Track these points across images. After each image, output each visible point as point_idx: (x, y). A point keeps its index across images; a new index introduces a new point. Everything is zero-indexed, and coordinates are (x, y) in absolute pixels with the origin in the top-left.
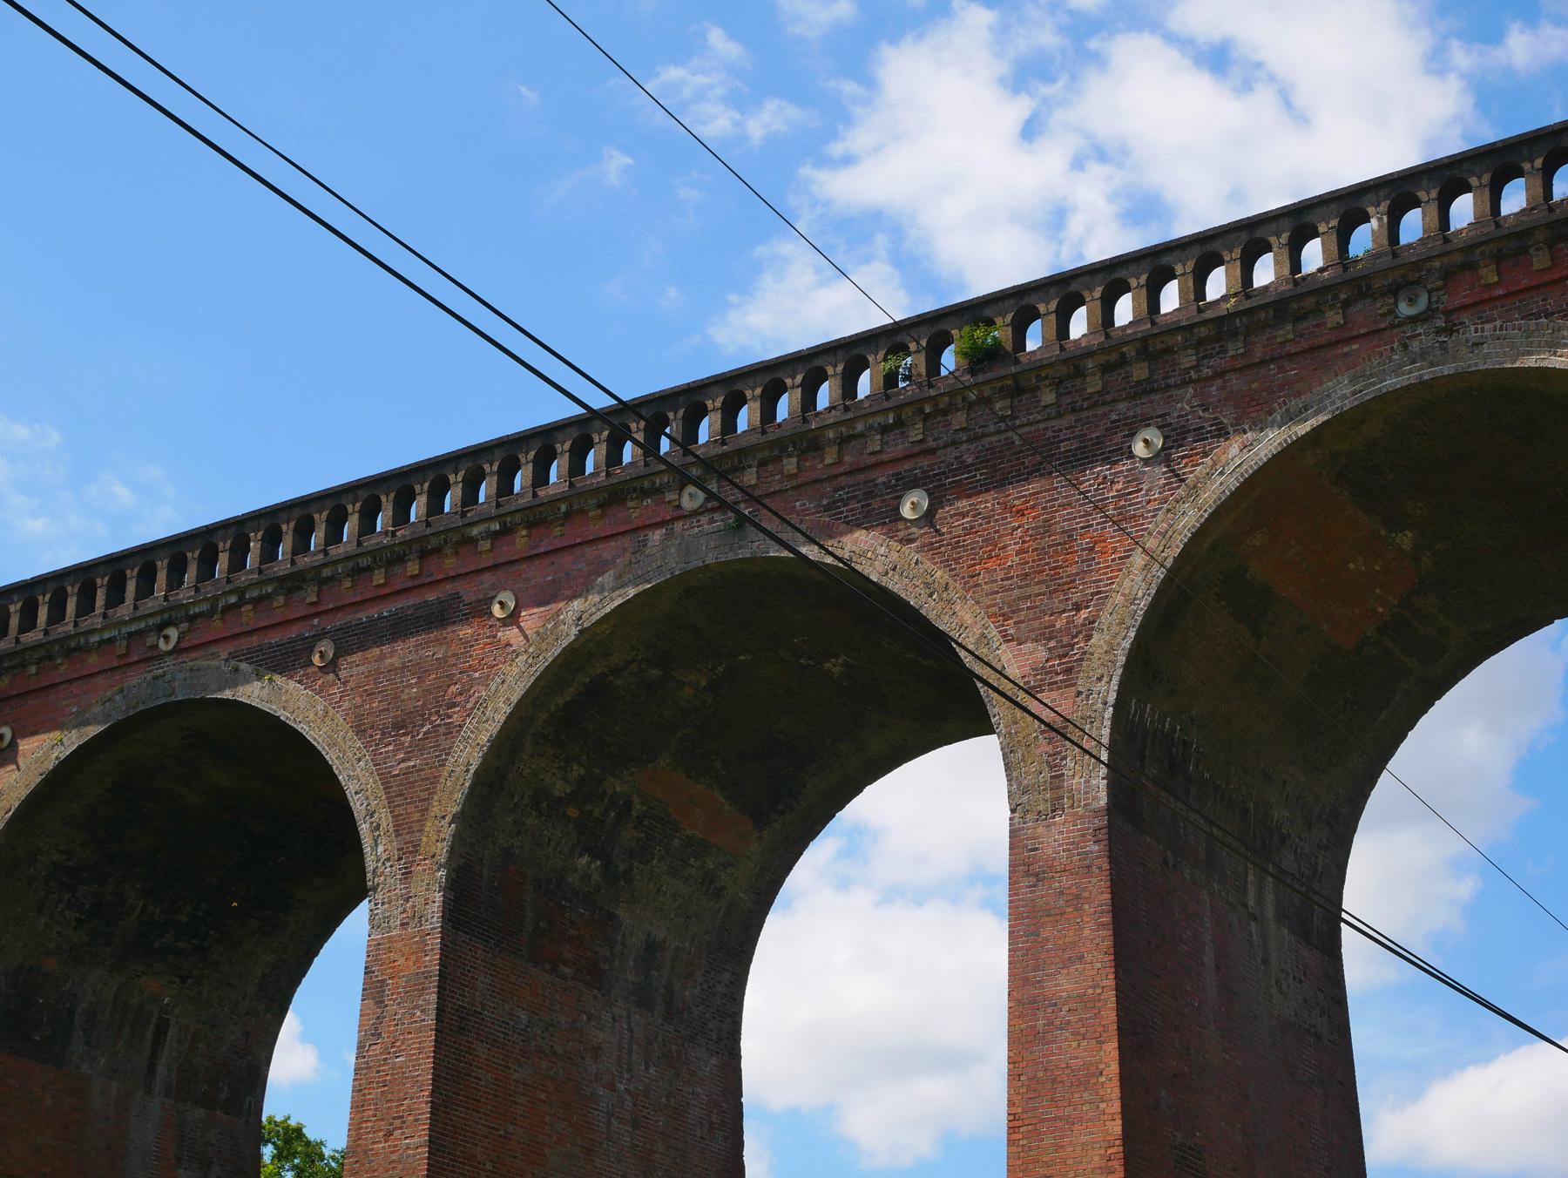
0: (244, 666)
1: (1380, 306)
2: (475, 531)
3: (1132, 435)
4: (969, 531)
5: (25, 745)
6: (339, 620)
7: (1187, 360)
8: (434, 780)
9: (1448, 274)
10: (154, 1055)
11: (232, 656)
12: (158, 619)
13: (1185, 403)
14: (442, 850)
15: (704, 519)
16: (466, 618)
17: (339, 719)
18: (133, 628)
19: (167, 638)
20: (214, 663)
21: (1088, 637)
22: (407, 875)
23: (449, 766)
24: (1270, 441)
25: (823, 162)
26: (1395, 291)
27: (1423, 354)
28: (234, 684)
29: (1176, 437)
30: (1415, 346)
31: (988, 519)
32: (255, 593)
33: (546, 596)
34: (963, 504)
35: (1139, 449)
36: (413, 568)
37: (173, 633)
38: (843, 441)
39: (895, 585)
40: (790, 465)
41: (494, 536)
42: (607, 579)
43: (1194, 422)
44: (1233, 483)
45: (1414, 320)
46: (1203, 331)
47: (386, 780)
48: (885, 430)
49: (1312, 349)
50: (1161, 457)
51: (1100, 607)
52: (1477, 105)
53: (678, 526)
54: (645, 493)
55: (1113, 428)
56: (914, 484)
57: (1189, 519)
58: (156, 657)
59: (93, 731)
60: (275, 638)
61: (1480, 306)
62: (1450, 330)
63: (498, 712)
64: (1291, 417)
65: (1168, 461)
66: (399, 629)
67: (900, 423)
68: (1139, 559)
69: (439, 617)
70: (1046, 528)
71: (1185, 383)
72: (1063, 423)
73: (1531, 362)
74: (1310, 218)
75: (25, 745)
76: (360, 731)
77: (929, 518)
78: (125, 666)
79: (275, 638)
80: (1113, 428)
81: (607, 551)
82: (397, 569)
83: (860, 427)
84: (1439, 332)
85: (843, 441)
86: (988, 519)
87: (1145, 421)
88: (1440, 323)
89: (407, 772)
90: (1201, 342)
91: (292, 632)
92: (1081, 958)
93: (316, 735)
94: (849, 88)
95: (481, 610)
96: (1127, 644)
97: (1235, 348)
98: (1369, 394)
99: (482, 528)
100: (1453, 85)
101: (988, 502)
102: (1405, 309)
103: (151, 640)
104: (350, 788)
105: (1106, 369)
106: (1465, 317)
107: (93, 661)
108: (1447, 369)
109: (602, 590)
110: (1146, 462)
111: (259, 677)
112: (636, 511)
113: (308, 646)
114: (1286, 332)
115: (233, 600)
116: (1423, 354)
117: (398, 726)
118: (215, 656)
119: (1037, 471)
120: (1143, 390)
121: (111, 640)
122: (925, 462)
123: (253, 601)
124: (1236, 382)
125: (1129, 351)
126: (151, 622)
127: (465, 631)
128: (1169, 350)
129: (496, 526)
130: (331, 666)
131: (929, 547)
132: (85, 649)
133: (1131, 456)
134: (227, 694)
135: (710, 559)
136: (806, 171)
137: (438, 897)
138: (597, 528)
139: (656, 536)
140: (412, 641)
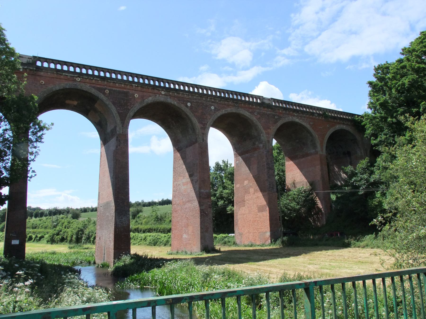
6: (111, 88)
15: (164, 96)
19: (78, 79)
37: (79, 79)
53: (160, 95)
79: (98, 86)
81: (151, 94)
87: (213, 105)
120: (213, 102)
139: (158, 95)
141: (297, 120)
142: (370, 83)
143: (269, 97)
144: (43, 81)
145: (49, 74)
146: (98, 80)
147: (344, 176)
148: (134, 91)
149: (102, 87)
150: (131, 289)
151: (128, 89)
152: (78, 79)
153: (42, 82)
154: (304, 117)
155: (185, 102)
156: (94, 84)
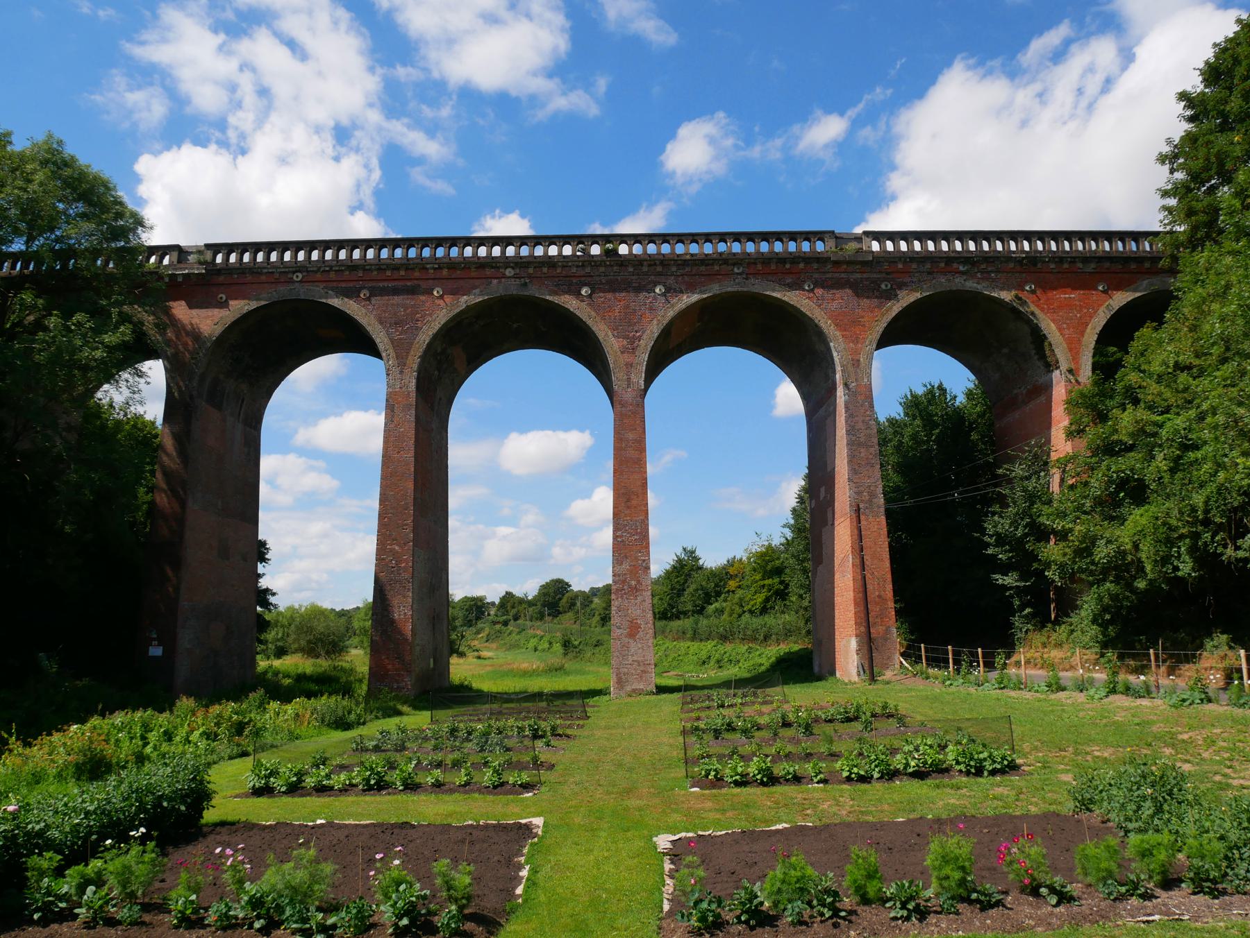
0: (330, 292)
1: (730, 268)
2: (428, 266)
3: (655, 286)
4: (603, 303)
5: (231, 302)
6: (374, 284)
7: (674, 269)
8: (412, 344)
9: (749, 264)
10: (241, 410)
11: (325, 288)
12: (294, 269)
13: (671, 281)
14: (415, 367)
15: (513, 280)
16: (423, 293)
17: (372, 317)
18: (283, 270)
19: (297, 276)
20: (318, 289)
21: (639, 341)
22: (401, 372)
23: (417, 340)
24: (695, 298)
25: (130, 40)
26: (734, 265)
27: (739, 284)
28: (327, 298)
29: (668, 290)
30: (737, 281)
31: (609, 300)
32: (337, 268)
33: (456, 292)
34: (602, 294)
35: (657, 290)
36: (402, 273)
37: (300, 276)
38: (564, 266)
39: (578, 313)
40: (545, 270)
41: (435, 269)
42: (477, 291)
43: (673, 287)
44: (684, 307)
45: (738, 274)
46: (680, 262)
47: (392, 341)
48: (578, 266)
49: (709, 275)
50: (664, 295)
51: (643, 332)
52: (385, 88)
53: (503, 280)
54: (493, 267)
55: (649, 283)
56: (585, 285)
57: (671, 314)
58: (291, 281)
59: (263, 303)
60: (344, 285)
61: (755, 274)
62: (747, 279)
63: (436, 326)
64: (701, 292)
65: (665, 296)
66: (396, 292)
67: (583, 266)
68: (655, 322)
69: (413, 291)
70: (627, 307)
71: (672, 275)
72: (634, 277)
73: (768, 293)
74: (711, 238)
75: (231, 302)
76: (381, 323)
77: (590, 296)
78: (277, 282)
79: (344, 285)
80: (649, 283)
81: (477, 282)
82: (395, 272)
83: (570, 264)
84: (744, 278)
85: (564, 267)
86: (609, 300)
87: (659, 283)
88: (744, 276)
89: (401, 339)
90: (679, 265)
91: (351, 285)
92: (636, 429)
93: (363, 321)
94: (148, 14)
95: (429, 292)
96: (651, 345)
97: (687, 269)
98: (723, 291)
99: (431, 265)
100: (377, 79)
101: (609, 295)
102: (736, 270)
103: (290, 276)
104: (378, 341)
105: (650, 265)
106: (751, 276)
107: (263, 278)
108: (745, 289)
109: (475, 295)
110: (659, 295)
111: (337, 297)
112: (488, 272)
113: (359, 291)
114: (703, 268)
115: (327, 269)
116: (739, 284)
117: (396, 324)
118: (317, 286)
119: (626, 290)
120: (660, 274)
121: (272, 273)
122: (589, 279)
123: (336, 271)
124: (686, 278)
125: (658, 262)
126: (291, 269)
127: (423, 298)
128: (669, 265)
129: (437, 266)
130: (368, 299)
131: (589, 304)
132: (261, 273)
133: (654, 292)
134: (324, 301)
135: (515, 292)
136: (123, 42)
137: (414, 381)
138: (473, 274)
139: (495, 281)
140: (402, 297)
141: (971, 285)
142: (1183, 96)
143: (201, 242)
144: (222, 293)
145: (236, 276)
146: (342, 270)
147: (1009, 580)
148: (431, 281)
149: (351, 285)
150: (395, 882)
151: (417, 279)
152: (297, 276)
153: (221, 298)
154: (997, 271)
155: (573, 288)
156: (417, 279)
